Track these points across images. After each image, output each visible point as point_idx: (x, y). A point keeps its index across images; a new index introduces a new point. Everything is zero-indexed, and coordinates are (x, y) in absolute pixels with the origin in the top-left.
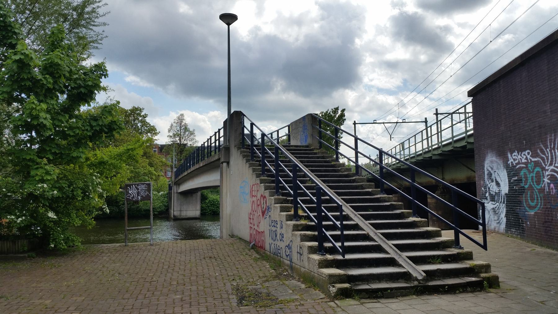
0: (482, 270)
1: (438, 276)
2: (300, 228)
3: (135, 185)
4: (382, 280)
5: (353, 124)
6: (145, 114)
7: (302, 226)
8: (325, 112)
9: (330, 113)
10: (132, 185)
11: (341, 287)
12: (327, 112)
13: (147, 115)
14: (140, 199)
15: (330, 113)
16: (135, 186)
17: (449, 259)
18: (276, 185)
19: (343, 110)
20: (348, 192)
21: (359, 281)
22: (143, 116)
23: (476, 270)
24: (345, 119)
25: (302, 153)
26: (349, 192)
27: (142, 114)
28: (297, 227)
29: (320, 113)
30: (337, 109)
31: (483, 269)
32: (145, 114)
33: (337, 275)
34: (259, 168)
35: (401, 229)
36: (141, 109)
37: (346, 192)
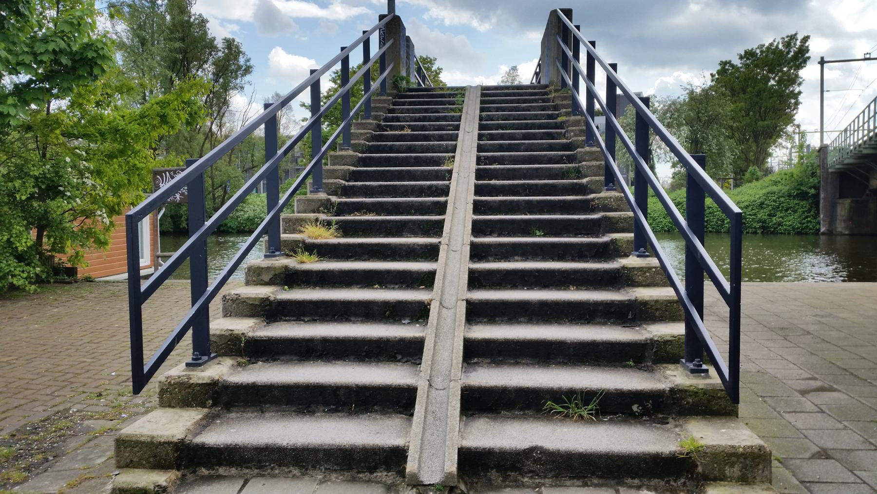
0: (728, 471)
1: (534, 473)
2: (266, 277)
3: (170, 171)
4: (314, 467)
5: (819, 63)
6: (438, 69)
7: (273, 273)
8: (767, 45)
9: (777, 46)
10: (165, 172)
11: (124, 486)
12: (771, 44)
13: (442, 69)
14: (178, 198)
15: (777, 47)
16: (170, 175)
17: (635, 408)
18: (605, 178)
19: (806, 39)
20: (518, 185)
21: (231, 463)
22: (436, 71)
23: (700, 469)
24: (809, 58)
25: (514, 100)
26: (523, 185)
27: (433, 69)
28: (259, 275)
29: (758, 48)
30: (793, 37)
31: (732, 465)
32: (438, 69)
33: (142, 443)
34: (361, 134)
35: (578, 289)
36: (431, 60)
37: (513, 185)
